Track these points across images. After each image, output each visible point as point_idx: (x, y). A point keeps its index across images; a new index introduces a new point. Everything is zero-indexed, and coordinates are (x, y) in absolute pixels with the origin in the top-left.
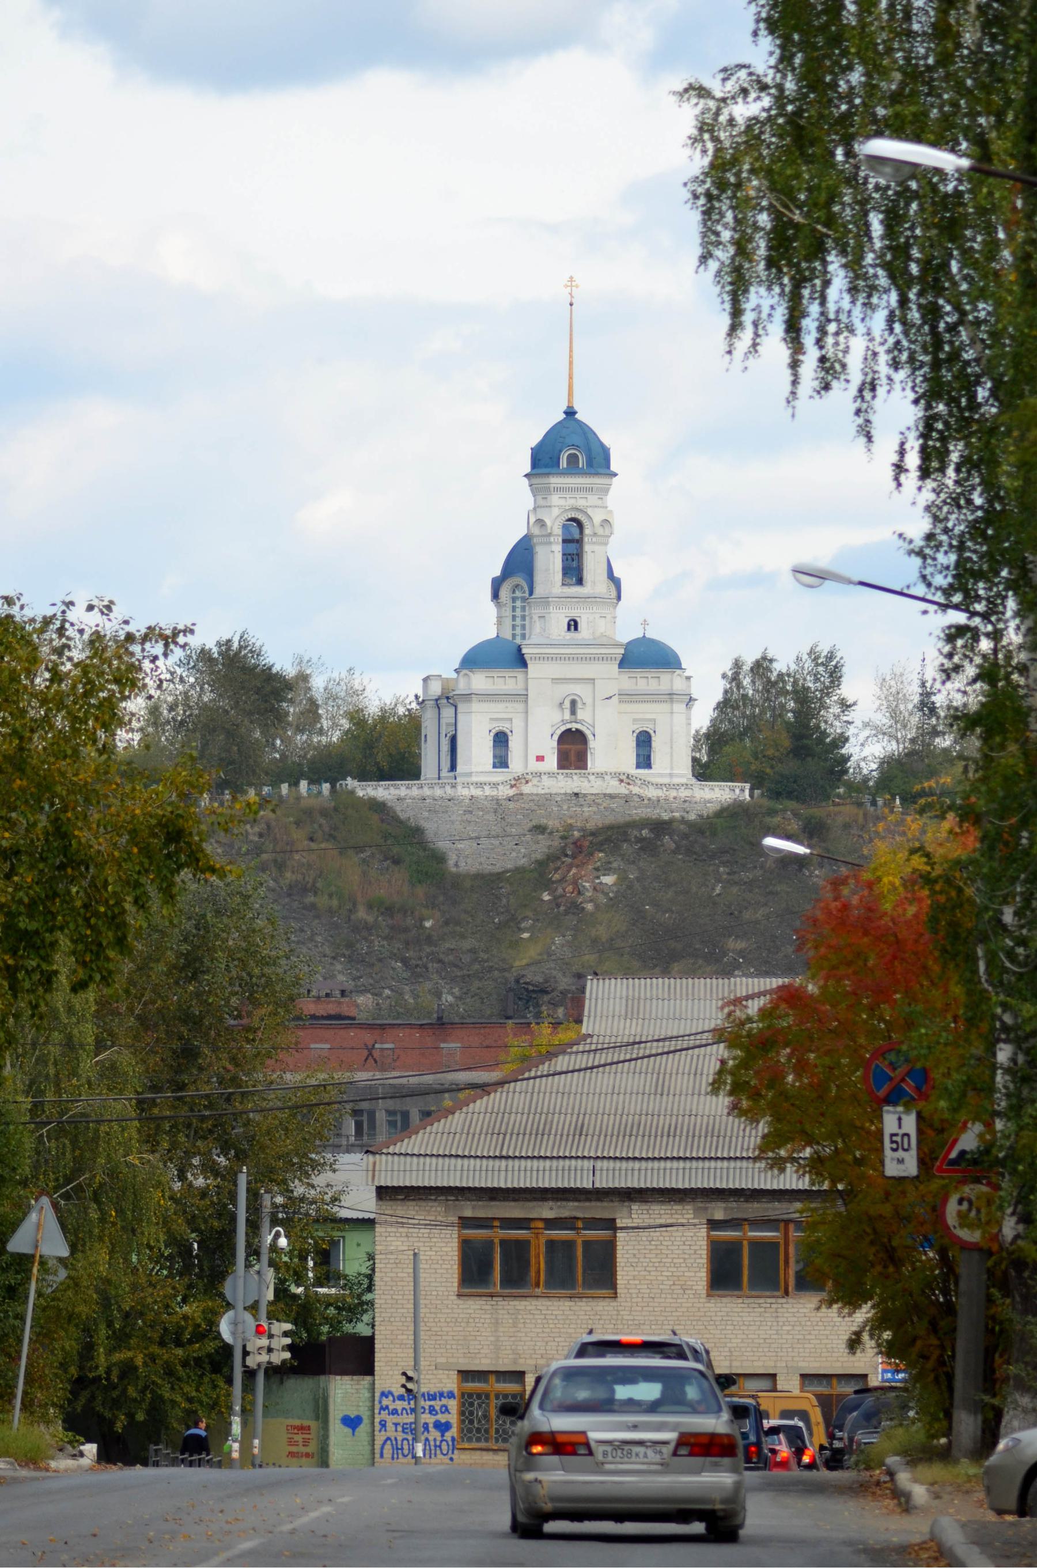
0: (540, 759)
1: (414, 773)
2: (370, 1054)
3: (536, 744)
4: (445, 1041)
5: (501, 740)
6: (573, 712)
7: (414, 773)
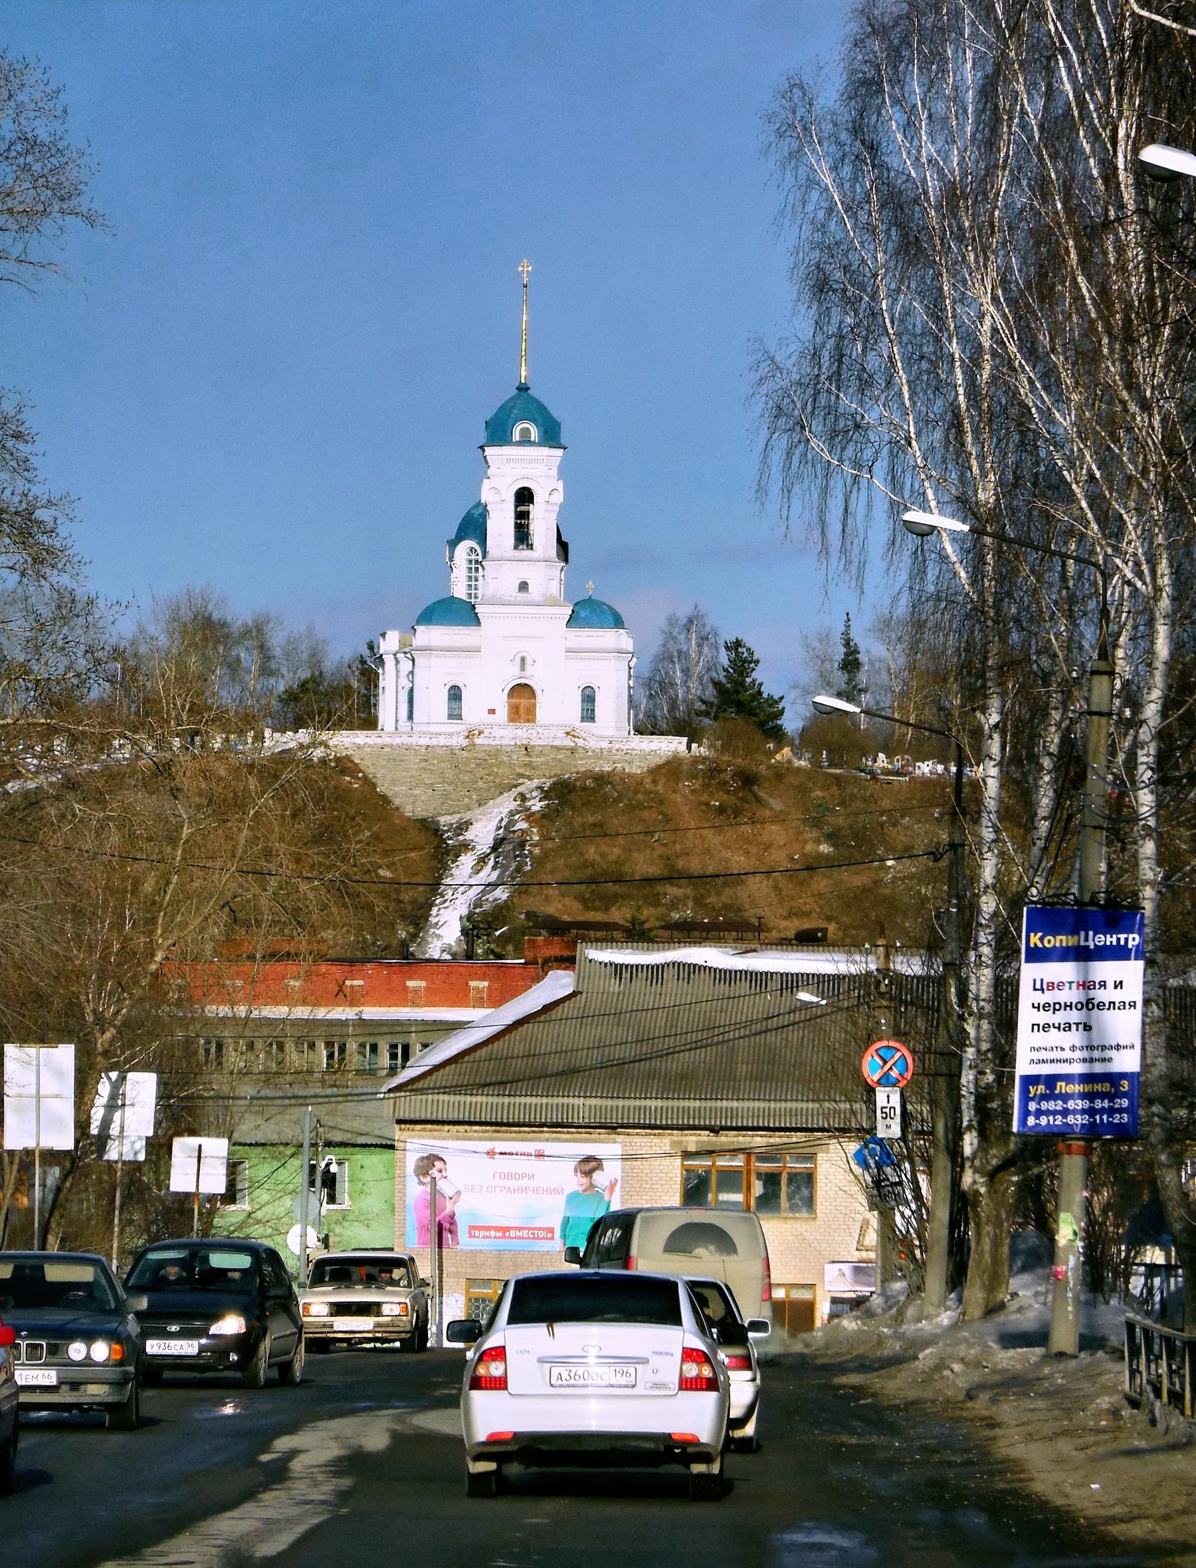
0: (492, 711)
1: (370, 723)
2: (341, 990)
3: (486, 699)
4: (412, 979)
5: (455, 694)
6: (523, 668)
7: (370, 723)
